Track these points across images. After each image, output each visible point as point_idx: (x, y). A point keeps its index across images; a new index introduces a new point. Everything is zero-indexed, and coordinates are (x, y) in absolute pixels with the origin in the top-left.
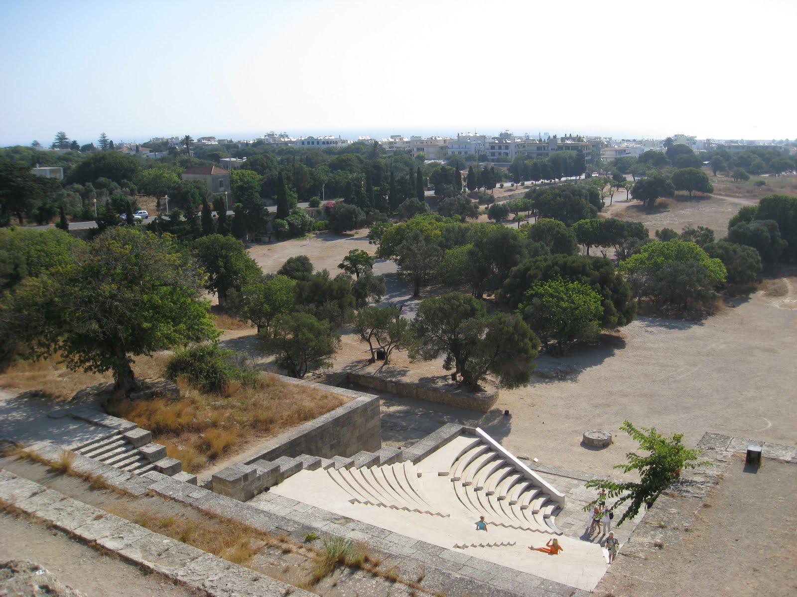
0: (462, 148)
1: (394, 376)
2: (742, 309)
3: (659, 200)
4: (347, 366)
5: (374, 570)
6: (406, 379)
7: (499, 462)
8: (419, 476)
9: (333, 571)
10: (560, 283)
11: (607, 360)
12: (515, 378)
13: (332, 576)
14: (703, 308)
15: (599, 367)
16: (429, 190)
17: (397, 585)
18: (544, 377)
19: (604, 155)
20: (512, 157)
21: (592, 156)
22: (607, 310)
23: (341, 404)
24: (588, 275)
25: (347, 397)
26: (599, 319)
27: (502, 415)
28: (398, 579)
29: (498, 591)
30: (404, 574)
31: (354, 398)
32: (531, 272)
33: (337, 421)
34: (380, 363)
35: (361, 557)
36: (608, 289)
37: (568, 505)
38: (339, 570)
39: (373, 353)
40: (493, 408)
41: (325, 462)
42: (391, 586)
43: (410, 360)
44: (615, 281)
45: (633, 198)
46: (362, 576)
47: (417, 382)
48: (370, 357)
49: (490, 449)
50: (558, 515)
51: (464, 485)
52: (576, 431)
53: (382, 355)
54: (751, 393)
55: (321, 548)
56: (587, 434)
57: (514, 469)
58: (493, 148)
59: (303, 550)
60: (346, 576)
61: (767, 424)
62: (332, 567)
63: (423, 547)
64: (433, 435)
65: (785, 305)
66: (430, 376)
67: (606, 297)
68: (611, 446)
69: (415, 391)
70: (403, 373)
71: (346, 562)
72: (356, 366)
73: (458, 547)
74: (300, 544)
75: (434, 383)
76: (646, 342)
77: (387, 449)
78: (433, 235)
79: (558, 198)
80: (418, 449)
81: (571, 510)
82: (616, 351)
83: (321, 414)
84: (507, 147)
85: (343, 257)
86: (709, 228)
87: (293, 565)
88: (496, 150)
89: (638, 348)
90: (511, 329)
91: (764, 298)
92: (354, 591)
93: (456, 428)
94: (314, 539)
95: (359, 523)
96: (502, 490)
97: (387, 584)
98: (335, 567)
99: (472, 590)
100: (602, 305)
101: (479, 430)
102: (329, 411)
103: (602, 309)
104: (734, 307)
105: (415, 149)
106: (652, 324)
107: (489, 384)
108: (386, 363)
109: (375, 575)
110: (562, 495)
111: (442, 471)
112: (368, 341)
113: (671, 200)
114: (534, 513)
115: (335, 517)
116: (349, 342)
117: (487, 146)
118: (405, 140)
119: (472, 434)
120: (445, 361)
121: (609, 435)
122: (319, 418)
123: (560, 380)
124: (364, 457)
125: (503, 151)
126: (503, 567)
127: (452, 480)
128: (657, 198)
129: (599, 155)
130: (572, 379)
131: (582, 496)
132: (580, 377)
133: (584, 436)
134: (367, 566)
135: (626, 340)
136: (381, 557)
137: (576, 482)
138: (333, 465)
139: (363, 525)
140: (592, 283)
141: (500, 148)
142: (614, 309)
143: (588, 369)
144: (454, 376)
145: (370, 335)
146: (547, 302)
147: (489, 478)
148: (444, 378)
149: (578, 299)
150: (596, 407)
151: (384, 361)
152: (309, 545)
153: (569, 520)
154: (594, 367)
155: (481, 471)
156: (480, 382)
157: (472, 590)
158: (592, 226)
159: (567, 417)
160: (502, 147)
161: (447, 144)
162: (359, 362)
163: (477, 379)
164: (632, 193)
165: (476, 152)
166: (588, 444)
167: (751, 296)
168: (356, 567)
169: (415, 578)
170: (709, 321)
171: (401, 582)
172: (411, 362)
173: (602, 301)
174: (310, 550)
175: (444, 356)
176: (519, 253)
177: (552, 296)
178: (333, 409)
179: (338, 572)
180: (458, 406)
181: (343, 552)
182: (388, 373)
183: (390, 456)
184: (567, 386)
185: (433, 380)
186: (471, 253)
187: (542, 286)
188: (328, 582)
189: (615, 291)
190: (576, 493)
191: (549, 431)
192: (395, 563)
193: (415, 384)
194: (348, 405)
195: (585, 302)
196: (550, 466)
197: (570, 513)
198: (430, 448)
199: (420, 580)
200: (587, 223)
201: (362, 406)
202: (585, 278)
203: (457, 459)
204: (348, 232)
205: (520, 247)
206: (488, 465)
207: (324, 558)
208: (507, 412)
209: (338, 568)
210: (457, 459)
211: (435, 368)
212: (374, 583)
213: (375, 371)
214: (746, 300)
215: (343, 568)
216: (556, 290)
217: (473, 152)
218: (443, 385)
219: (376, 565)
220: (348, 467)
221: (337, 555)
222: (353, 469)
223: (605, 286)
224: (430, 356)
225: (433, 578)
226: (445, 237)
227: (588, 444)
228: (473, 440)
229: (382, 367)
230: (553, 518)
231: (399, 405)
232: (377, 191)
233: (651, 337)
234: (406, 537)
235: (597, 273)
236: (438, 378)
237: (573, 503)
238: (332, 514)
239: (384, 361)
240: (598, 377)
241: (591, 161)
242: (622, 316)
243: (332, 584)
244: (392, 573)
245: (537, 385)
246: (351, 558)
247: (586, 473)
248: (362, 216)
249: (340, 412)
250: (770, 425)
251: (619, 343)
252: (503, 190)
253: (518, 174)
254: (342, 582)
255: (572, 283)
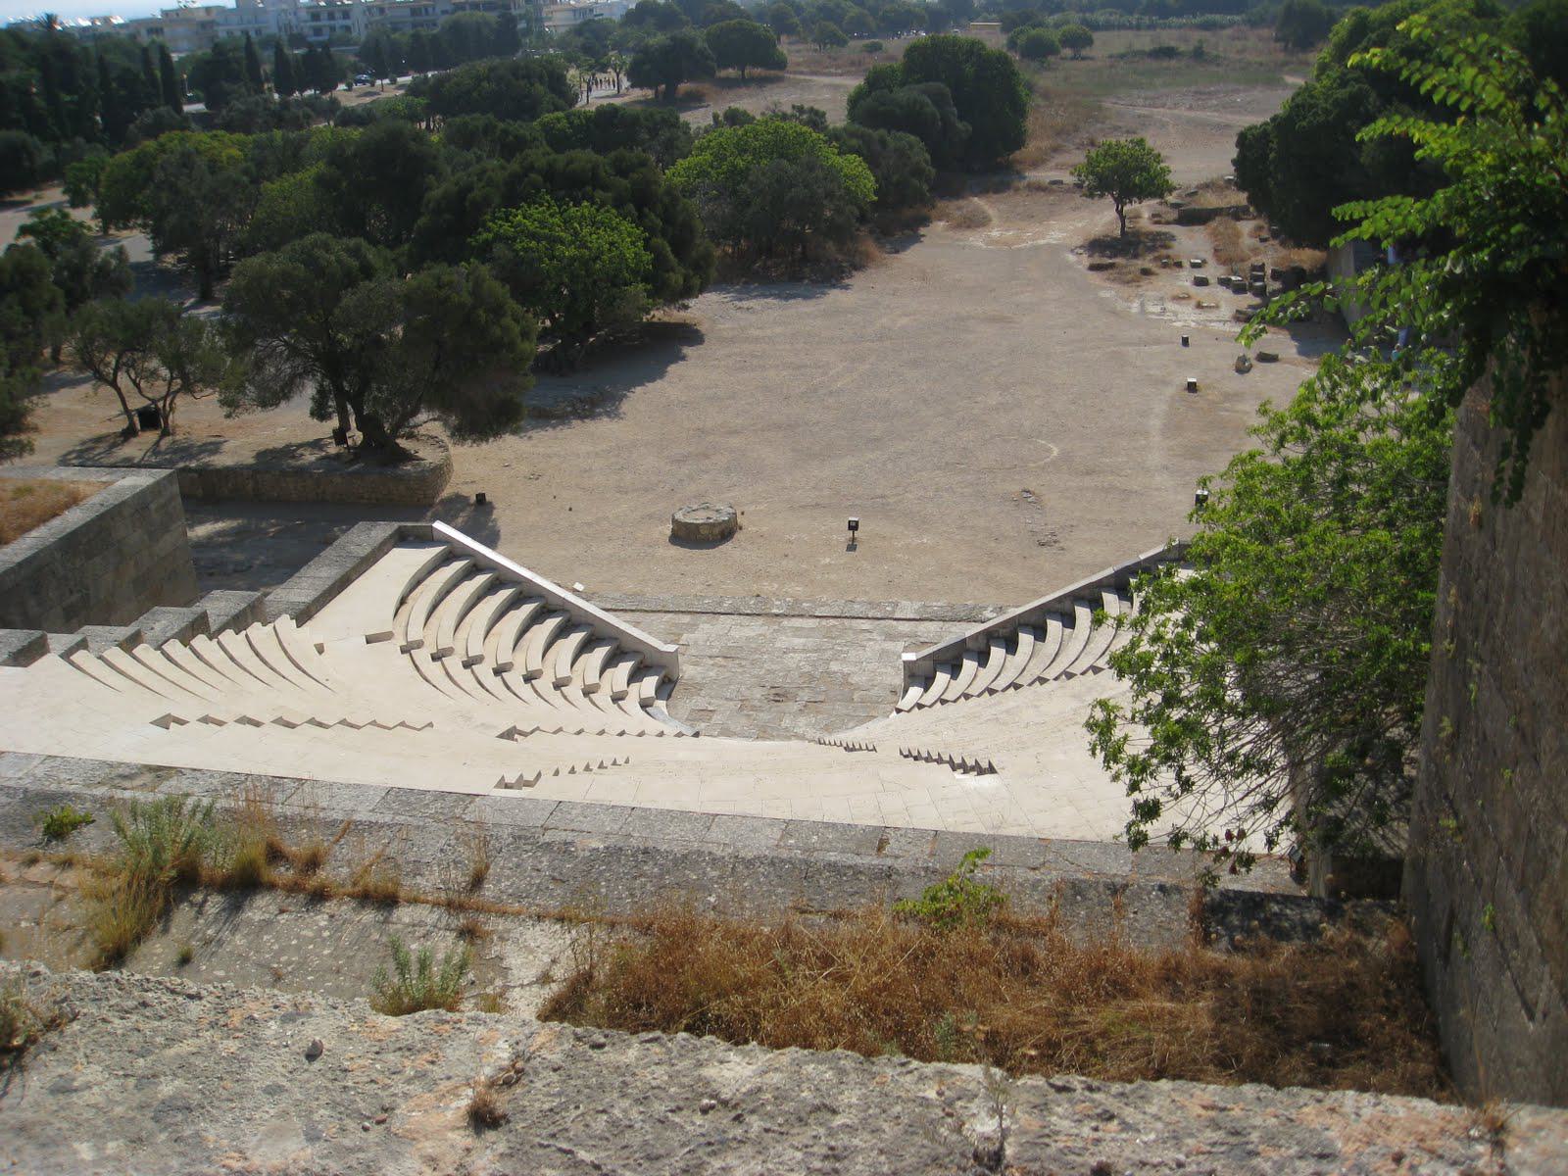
0: (249, 22)
1: (192, 457)
2: (912, 255)
3: (684, 87)
4: (70, 453)
5: (313, 882)
6: (221, 461)
7: (504, 594)
8: (320, 649)
9: (165, 914)
10: (549, 208)
11: (673, 369)
12: (483, 421)
13: (166, 931)
14: (840, 257)
15: (659, 383)
16: (191, 101)
17: (404, 914)
18: (546, 417)
19: (550, 19)
20: (360, 34)
21: (528, 22)
22: (659, 260)
23: (74, 500)
24: (605, 188)
25: (88, 483)
26: (645, 280)
27: (470, 505)
28: (402, 894)
29: (749, 863)
30: (417, 873)
31: (107, 484)
32: (476, 194)
33: (71, 542)
34: (151, 436)
35: (256, 852)
36: (653, 216)
37: (687, 671)
38: (185, 906)
39: (130, 417)
40: (447, 492)
41: (58, 641)
42: (386, 921)
43: (226, 410)
44: (666, 200)
45: (633, 86)
46: (273, 909)
47: (251, 461)
48: (125, 425)
49: (477, 566)
50: (669, 696)
51: (435, 658)
52: (650, 516)
53: (151, 418)
54: (994, 399)
55: (107, 850)
56: (679, 516)
57: (543, 607)
58: (315, 17)
59: (38, 872)
60: (216, 920)
61: (1049, 450)
62: (160, 903)
63: (409, 804)
64: (329, 553)
65: (992, 242)
66: (280, 444)
67: (651, 230)
68: (738, 535)
69: (250, 485)
70: (214, 448)
71: (204, 873)
72: (93, 449)
73: (507, 786)
74: (30, 852)
75: (294, 457)
76: (742, 334)
77: (220, 604)
78: (224, 158)
79: (485, 84)
80: (300, 589)
81: (699, 680)
82: (687, 350)
83: (24, 530)
84: (346, 15)
85: (15, 231)
86: (816, 107)
87: (17, 924)
88: (324, 22)
89: (732, 340)
90: (467, 299)
91: (951, 233)
92: (259, 965)
93: (383, 530)
94: (75, 825)
95: (198, 774)
96: (532, 652)
97: (369, 916)
98: (167, 901)
99: (661, 876)
100: (646, 247)
101: (439, 525)
102: (43, 520)
103: (648, 257)
104: (897, 252)
105: (143, 32)
106: (745, 293)
107: (429, 438)
108: (165, 433)
109: (319, 896)
110: (671, 648)
111: (372, 632)
112: (114, 384)
113: (707, 86)
114: (617, 698)
115: (120, 771)
116: (64, 405)
117: (303, 15)
118: (115, 21)
119: (425, 539)
120: (313, 398)
121: (731, 511)
122: (20, 540)
123: (582, 418)
124: (166, 619)
125: (340, 22)
126: (661, 812)
127: (405, 650)
128: (680, 81)
129: (540, 20)
130: (608, 414)
131: (711, 647)
132: (625, 406)
133: (675, 521)
134: (283, 874)
135: (702, 328)
136: (321, 839)
137: (686, 619)
138: (83, 645)
139: (212, 776)
140: (619, 204)
141: (331, 16)
142: (672, 257)
143: (639, 389)
144: (340, 436)
145: (116, 370)
146: (525, 250)
147: (491, 633)
148: (317, 444)
149: (598, 240)
150: (679, 461)
151: (159, 432)
152: (60, 850)
153: (700, 702)
154: (650, 385)
155: (467, 619)
156: (403, 443)
157: (661, 876)
158: (571, 123)
159: (622, 490)
160: (337, 15)
161: (213, 16)
162: (99, 440)
163: (395, 433)
164: (630, 75)
165: (280, 29)
166: (687, 536)
167: (922, 231)
168: (243, 885)
169: (459, 877)
170: (858, 280)
171: (414, 901)
172: (228, 416)
173: (647, 241)
174: (67, 864)
175: (310, 389)
176: (434, 171)
177: (533, 236)
178: (55, 515)
179: (183, 914)
180: (373, 492)
181: (189, 842)
182: (175, 452)
183: (234, 612)
184: (602, 428)
185: (288, 451)
186: (320, 180)
187: (507, 221)
188: (158, 951)
189: (668, 219)
190: (696, 643)
191: (589, 524)
192: (372, 847)
193: (249, 467)
194: (96, 499)
195: (612, 244)
196: (617, 595)
197: (696, 688)
198: (330, 583)
199: (477, 881)
200: (558, 120)
201: (134, 496)
202: (599, 195)
203: (403, 601)
204: (17, 198)
205: (435, 158)
206: (481, 605)
207: (122, 880)
208: (481, 499)
209: (179, 900)
210: (403, 601)
211: (295, 424)
212: (323, 924)
213: (142, 453)
214: (916, 239)
215: (199, 897)
216: (543, 224)
217: (273, 30)
218: (318, 459)
219: (313, 863)
220: (129, 644)
221: (168, 855)
222: (139, 651)
223: (646, 210)
224: (273, 396)
225: (518, 866)
226: (252, 160)
227: (687, 536)
228: (429, 553)
229: (157, 443)
230: (661, 704)
231: (217, 521)
232: (71, 102)
233: (753, 318)
234: (348, 786)
235: (625, 183)
236: (300, 446)
237: (696, 664)
238: (111, 766)
239: (159, 432)
240: (653, 406)
241: (527, 32)
242: (691, 272)
243: (175, 958)
244: (373, 880)
245: (534, 434)
246: (218, 861)
247: (705, 597)
248: (46, 155)
249: (74, 518)
250: (1056, 452)
251: (689, 335)
252: (353, 94)
253: (380, 59)
254: (208, 942)
255: (577, 204)
